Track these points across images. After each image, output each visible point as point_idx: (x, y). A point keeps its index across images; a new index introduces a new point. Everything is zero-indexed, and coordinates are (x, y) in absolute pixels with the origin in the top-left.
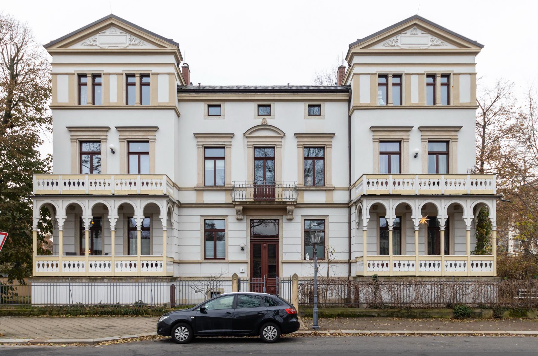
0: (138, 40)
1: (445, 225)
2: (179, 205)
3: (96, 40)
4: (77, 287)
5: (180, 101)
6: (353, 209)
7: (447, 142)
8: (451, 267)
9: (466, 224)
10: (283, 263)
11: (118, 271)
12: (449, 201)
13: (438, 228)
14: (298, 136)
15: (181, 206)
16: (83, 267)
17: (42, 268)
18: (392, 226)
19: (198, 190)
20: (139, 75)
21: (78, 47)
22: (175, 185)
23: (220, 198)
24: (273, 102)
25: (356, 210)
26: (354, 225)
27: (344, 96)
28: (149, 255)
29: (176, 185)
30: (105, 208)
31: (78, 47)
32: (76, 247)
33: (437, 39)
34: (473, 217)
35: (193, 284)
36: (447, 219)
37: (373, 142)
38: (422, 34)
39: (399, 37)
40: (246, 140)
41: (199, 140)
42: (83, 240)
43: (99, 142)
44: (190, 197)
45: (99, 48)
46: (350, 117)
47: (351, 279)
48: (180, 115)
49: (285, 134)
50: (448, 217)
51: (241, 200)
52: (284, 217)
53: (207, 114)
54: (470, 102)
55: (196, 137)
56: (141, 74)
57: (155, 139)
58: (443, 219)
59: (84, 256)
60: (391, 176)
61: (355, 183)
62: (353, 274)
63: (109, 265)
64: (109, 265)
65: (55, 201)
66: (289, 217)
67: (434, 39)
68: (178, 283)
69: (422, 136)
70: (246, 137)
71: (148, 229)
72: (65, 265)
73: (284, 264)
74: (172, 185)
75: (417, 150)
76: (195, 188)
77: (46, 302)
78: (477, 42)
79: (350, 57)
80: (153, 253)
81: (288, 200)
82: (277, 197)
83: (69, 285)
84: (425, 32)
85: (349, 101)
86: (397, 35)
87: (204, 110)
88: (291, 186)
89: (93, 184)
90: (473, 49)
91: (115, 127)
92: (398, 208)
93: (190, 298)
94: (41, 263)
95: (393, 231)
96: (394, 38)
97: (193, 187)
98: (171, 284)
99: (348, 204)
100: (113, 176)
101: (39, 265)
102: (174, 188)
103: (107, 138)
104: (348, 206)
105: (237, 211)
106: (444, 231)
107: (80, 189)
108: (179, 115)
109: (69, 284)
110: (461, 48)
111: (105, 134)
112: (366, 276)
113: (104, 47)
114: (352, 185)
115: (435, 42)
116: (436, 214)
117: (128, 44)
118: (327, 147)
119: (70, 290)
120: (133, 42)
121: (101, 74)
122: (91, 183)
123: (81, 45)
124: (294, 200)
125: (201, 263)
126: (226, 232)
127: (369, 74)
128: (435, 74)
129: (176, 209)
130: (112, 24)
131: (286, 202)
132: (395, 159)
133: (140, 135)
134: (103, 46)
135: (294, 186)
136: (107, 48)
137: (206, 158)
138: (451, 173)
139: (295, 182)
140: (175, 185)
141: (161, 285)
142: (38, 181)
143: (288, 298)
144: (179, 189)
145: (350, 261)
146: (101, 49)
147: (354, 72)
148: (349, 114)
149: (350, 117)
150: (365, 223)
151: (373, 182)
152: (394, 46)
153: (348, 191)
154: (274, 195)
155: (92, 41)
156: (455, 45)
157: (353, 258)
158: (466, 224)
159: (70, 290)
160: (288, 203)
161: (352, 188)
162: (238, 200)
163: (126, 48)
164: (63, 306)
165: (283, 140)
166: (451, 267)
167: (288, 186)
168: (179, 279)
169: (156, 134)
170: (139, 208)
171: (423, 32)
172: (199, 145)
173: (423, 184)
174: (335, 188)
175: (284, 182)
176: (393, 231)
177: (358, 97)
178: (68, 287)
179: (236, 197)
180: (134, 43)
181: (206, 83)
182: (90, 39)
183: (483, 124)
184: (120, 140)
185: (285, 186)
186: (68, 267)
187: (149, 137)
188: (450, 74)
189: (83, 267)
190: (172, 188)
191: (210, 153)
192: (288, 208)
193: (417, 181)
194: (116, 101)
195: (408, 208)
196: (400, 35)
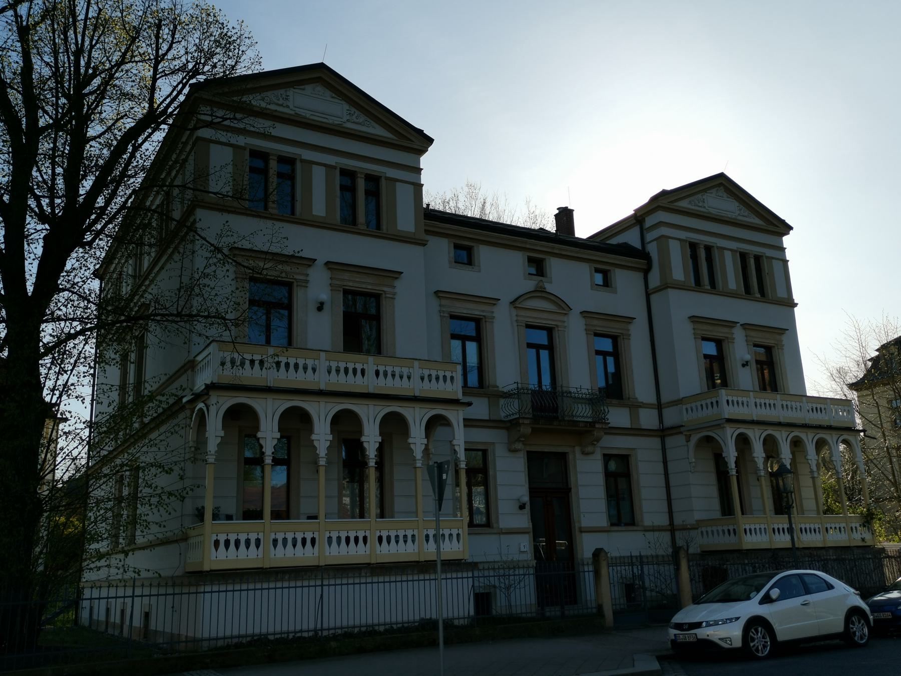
0: (362, 118)
1: (326, 455)
4: (223, 595)
8: (357, 545)
9: (318, 452)
10: (581, 532)
11: (391, 552)
13: (364, 464)
14: (585, 314)
16: (258, 546)
17: (412, 543)
18: (270, 454)
27: (642, 263)
28: (289, 519)
33: (357, 113)
34: (425, 441)
35: (481, 575)
36: (380, 443)
38: (333, 97)
39: (291, 92)
40: (514, 312)
41: (444, 302)
42: (366, 486)
45: (292, 112)
50: (382, 440)
56: (367, 174)
57: (395, 294)
59: (263, 521)
63: (313, 541)
64: (313, 541)
77: (345, 624)
83: (322, 586)
84: (336, 96)
86: (288, 89)
87: (449, 253)
93: (518, 603)
95: (376, 468)
96: (699, 196)
101: (217, 544)
103: (330, 281)
109: (471, 577)
113: (304, 114)
115: (354, 117)
116: (360, 432)
130: (721, 184)
134: (711, 210)
136: (308, 116)
142: (327, 363)
146: (710, 213)
150: (212, 445)
151: (430, 376)
152: (701, 207)
153: (657, 410)
155: (281, 99)
158: (318, 452)
163: (342, 124)
164: (403, 626)
166: (357, 545)
169: (397, 283)
171: (334, 95)
172: (444, 312)
176: (376, 468)
180: (355, 120)
187: (385, 289)
189: (258, 546)
196: (292, 89)
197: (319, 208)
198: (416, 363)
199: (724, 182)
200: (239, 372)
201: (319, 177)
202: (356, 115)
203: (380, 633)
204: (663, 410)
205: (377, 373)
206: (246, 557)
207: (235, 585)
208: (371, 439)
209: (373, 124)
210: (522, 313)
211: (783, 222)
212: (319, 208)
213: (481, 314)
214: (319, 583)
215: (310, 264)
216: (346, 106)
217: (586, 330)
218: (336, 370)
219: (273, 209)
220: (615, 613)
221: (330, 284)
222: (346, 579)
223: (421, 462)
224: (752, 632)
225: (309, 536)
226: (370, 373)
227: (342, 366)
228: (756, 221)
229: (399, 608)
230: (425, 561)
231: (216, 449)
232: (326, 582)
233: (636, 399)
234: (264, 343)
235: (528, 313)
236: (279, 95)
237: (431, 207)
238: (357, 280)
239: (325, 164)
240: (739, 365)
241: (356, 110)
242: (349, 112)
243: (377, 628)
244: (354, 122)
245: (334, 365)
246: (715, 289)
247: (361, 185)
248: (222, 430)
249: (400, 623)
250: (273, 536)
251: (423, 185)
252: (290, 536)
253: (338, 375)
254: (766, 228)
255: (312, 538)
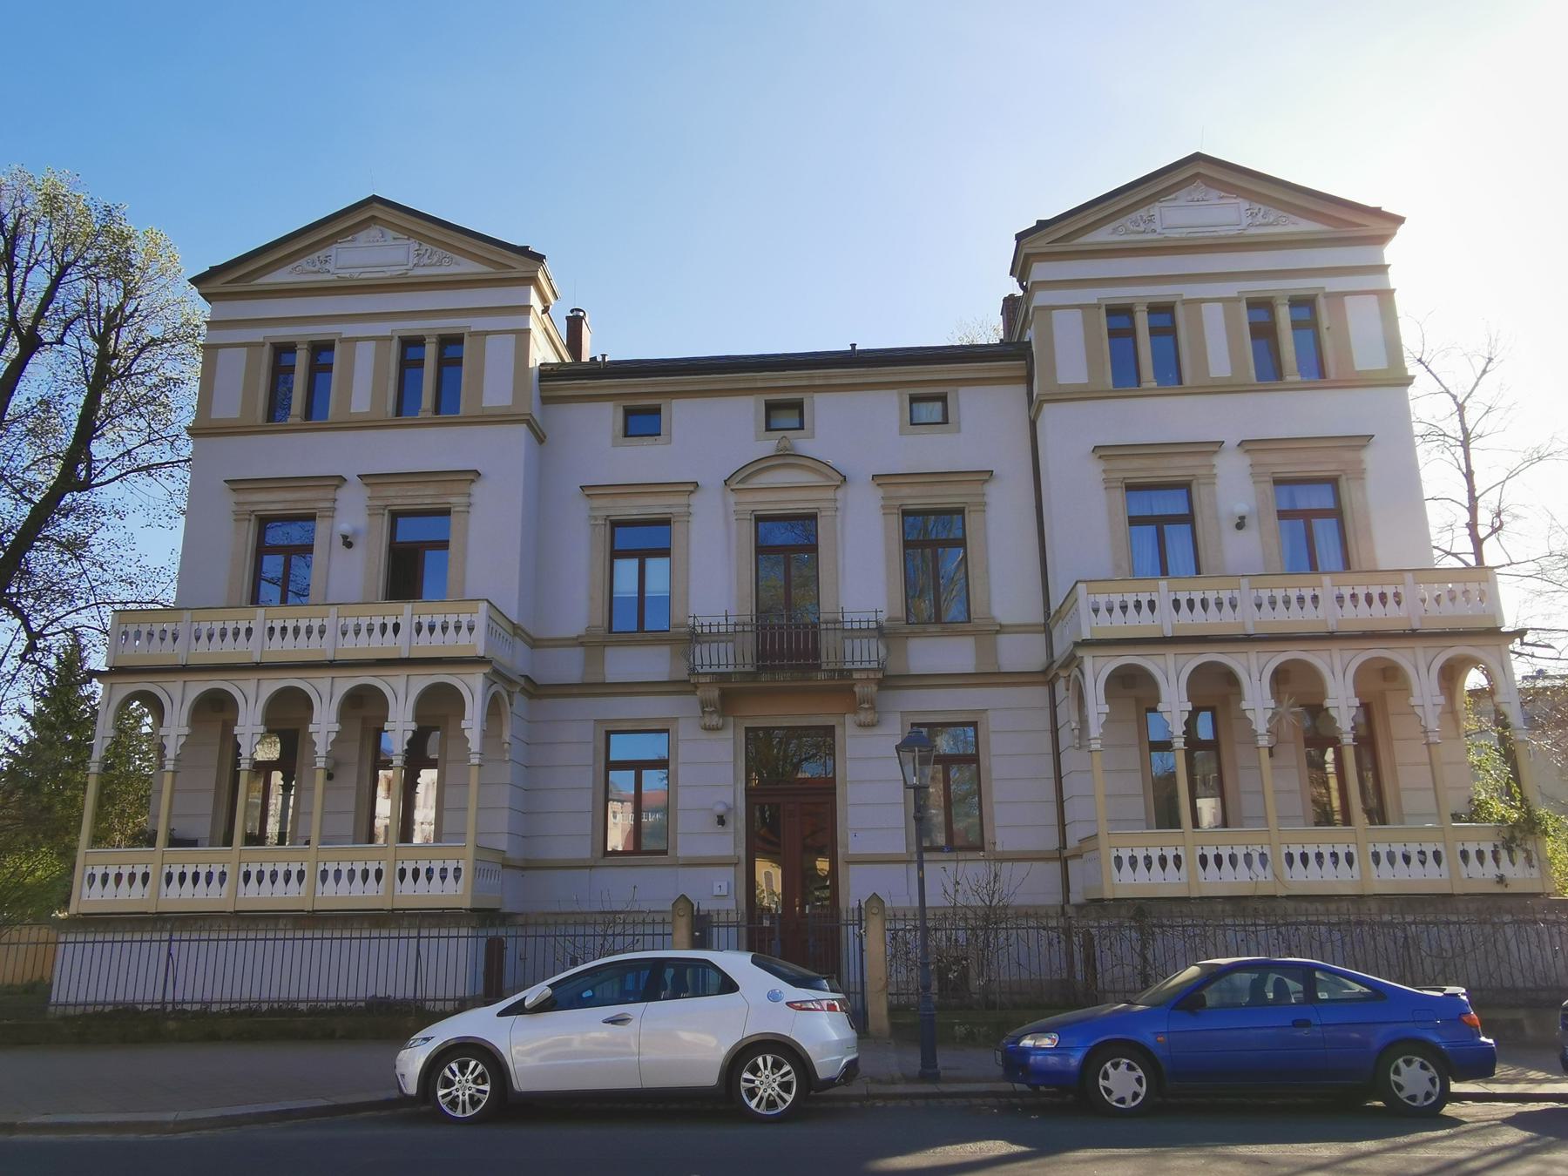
0: (1273, 214)
1: (1184, 733)
2: (531, 690)
3: (328, 259)
4: (453, 942)
5: (546, 400)
6: (1060, 686)
7: (1333, 482)
10: (848, 863)
11: (1309, 879)
12: (1189, 657)
15: (535, 690)
16: (457, 878)
19: (591, 644)
20: (434, 340)
21: (1102, 236)
22: (519, 631)
23: (651, 663)
24: (810, 394)
25: (1068, 690)
26: (1065, 737)
27: (1015, 367)
29: (523, 631)
30: (1230, 679)
31: (1102, 236)
32: (213, 824)
37: (235, 520)
40: (732, 498)
41: (597, 502)
43: (311, 518)
44: (568, 667)
45: (335, 277)
46: (1033, 425)
47: (1070, 911)
48: (545, 437)
49: (697, 483)
51: (714, 669)
52: (849, 718)
53: (622, 432)
54: (1087, 382)
55: (588, 495)
56: (440, 335)
58: (1343, 708)
59: (1182, 830)
60: (260, 612)
61: (1061, 607)
62: (1076, 898)
65: (463, 677)
66: (864, 717)
67: (1256, 211)
68: (511, 932)
69: (1104, 471)
70: (732, 490)
71: (1213, 746)
72: (1203, 860)
73: (851, 866)
74: (510, 630)
75: (1241, 508)
76: (580, 641)
78: (1383, 209)
79: (1020, 268)
80: (443, 838)
81: (857, 666)
82: (824, 658)
83: (171, 941)
84: (1226, 195)
85: (1029, 380)
88: (864, 625)
89: (1266, 606)
90: (520, 267)
91: (359, 476)
92: (1362, 673)
94: (99, 871)
95: (1355, 746)
97: (575, 635)
98: (492, 932)
99: (1044, 672)
100: (1410, 575)
102: (517, 639)
104: (1046, 677)
105: (704, 704)
106: (1183, 752)
107: (238, 649)
108: (540, 438)
110: (498, 269)
111: (330, 494)
112: (1110, 900)
114: (1052, 614)
116: (1323, 694)
117: (411, 265)
118: (972, 508)
119: (170, 954)
120: (1260, 219)
121: (334, 340)
122: (272, 629)
123: (1112, 234)
124: (874, 665)
125: (591, 867)
126: (670, 767)
127: (1078, 307)
128: (1272, 297)
129: (520, 701)
130: (1197, 176)
131: (850, 671)
132: (1177, 538)
133: (425, 497)
134: (345, 274)
135: (872, 625)
136: (356, 276)
137: (616, 554)
138: (1357, 569)
139: (876, 612)
140: (519, 631)
141: (458, 937)
143: (852, 979)
144: (535, 643)
145: (1066, 853)
146: (1167, 239)
147: (1036, 305)
148: (1030, 418)
149: (1033, 425)
150: (1095, 730)
154: (816, 653)
156: (1314, 220)
157: (1072, 843)
159: (170, 954)
160: (856, 676)
161: (1054, 627)
162: (706, 669)
163: (406, 273)
165: (840, 493)
167: (856, 626)
168: (520, 920)
170: (251, 701)
171: (1223, 194)
172: (595, 518)
173: (1266, 605)
174: (1001, 626)
175: (843, 613)
176: (1355, 746)
177: (1052, 369)
178: (413, 942)
179: (698, 662)
181: (619, 352)
182: (315, 256)
183: (1453, 428)
184: (1105, 483)
185: (848, 626)
186: (205, 884)
187: (453, 500)
188: (1317, 295)
190: (510, 639)
191: (627, 538)
192: (856, 689)
193: (332, 619)
194: (366, 409)
195: (1390, 673)
196: (1157, 204)
197: (1219, 365)
198: (1244, 582)
199: (1202, 170)
200: (1281, 613)
201: (1213, 318)
202: (1262, 212)
203: (300, 1013)
204: (973, 638)
205: (1176, 604)
206: (257, 896)
207: (460, 929)
208: (1342, 703)
209: (1293, 218)
210: (749, 497)
211: (1377, 213)
212: (1219, 365)
213: (667, 510)
214: (414, 933)
215: (1217, 449)
216: (1244, 204)
217: (883, 507)
218: (1121, 607)
219: (1292, 376)
220: (893, 1010)
221: (1251, 474)
222: (456, 929)
223: (1100, 741)
224: (451, 1070)
225: (217, 869)
226: (1164, 604)
227: (1293, 594)
228: (467, 267)
229: (392, 972)
230: (1114, 899)
231: (1185, 729)
232: (176, 936)
233: (993, 618)
234: (1341, 568)
235: (760, 497)
236: (1139, 218)
237: (857, 348)
238: (409, 494)
239: (245, 343)
240: (1228, 525)
241: (1261, 206)
242: (1249, 212)
243: (140, 1007)
244: (1259, 225)
245: (1265, 594)
246: (1324, 377)
247: (1142, 322)
248: (1107, 703)
249: (333, 1001)
250: (1371, 849)
251: (1394, 290)
252: (345, 867)
253: (1124, 613)
254: (1332, 236)
255: (299, 872)
